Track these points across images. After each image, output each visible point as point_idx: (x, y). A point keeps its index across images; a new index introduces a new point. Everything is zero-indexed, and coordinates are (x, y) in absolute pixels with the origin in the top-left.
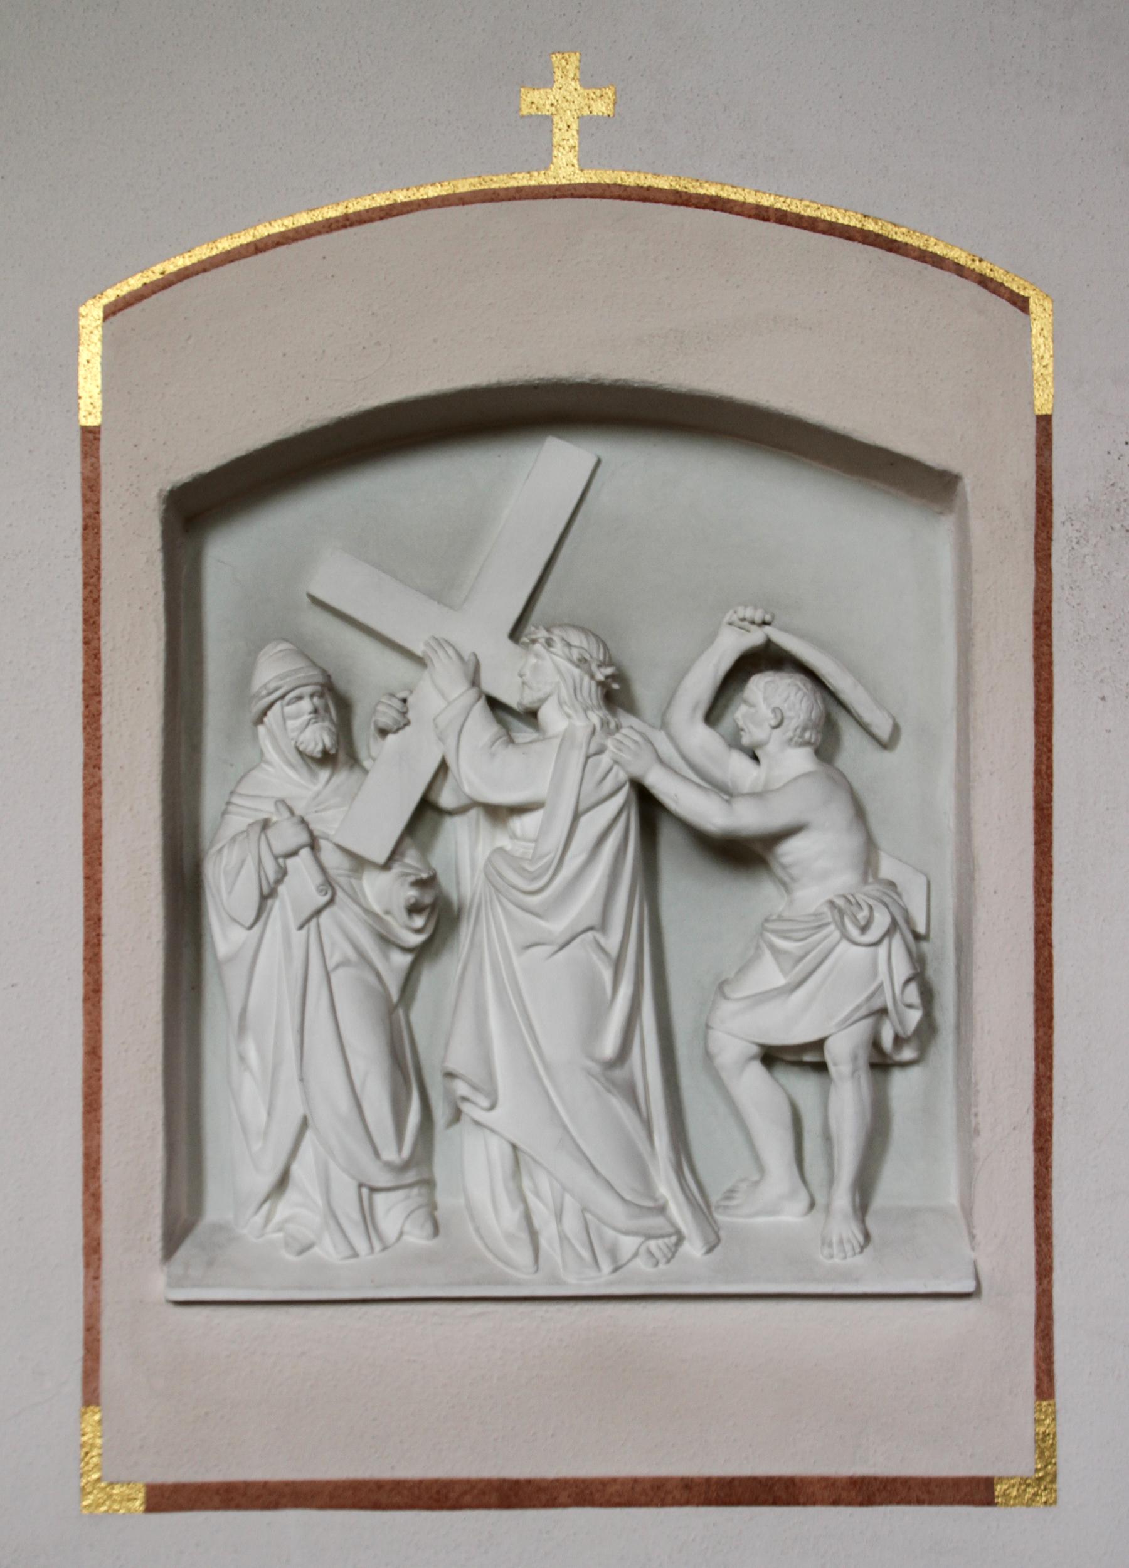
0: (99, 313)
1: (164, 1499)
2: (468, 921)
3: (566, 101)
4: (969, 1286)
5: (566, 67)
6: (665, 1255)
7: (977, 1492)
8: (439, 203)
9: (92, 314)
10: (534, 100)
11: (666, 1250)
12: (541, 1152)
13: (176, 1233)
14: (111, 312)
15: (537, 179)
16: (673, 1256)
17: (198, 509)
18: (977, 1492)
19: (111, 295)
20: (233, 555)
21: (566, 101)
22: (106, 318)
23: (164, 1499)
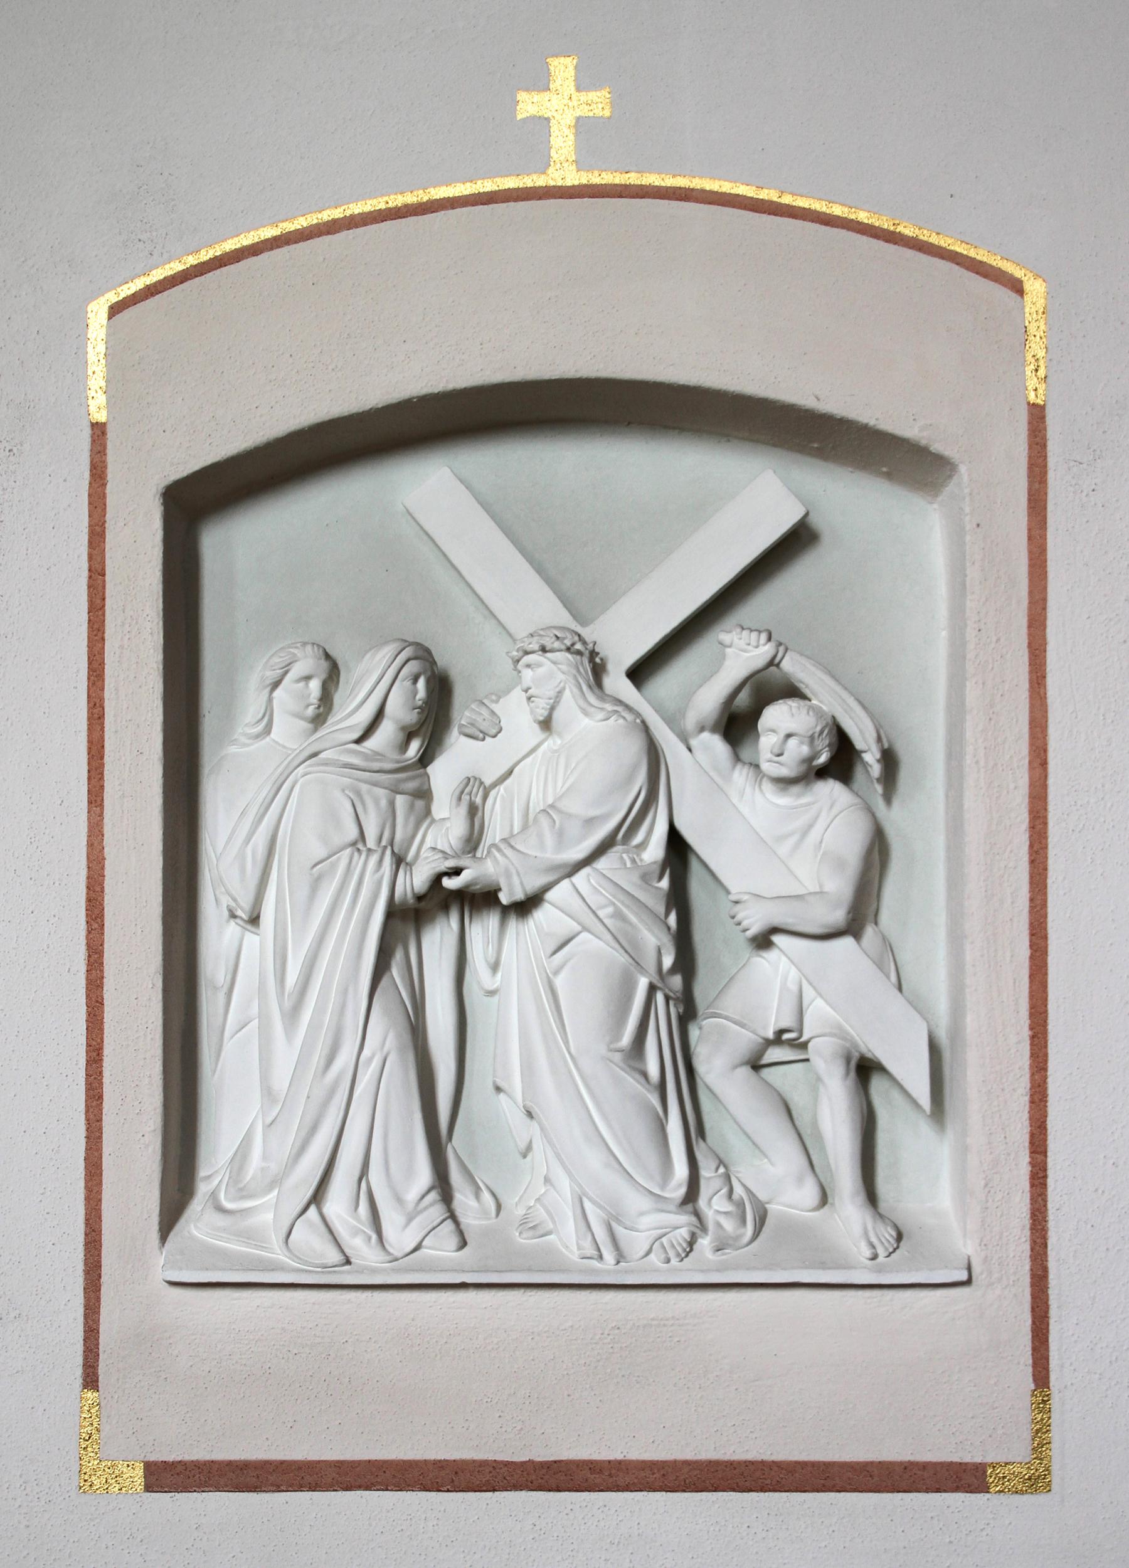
0: (104, 315)
1: (163, 1477)
2: (623, 903)
3: (562, 104)
4: (963, 1276)
5: (563, 69)
6: (685, 1250)
7: (966, 1478)
8: (95, 665)
9: (98, 312)
10: (528, 104)
11: (685, 1245)
12: (565, 1142)
13: (172, 1211)
14: (115, 310)
15: (540, 181)
16: (691, 1250)
17: (196, 503)
18: (966, 1478)
19: (112, 297)
20: (236, 545)
21: (562, 104)
22: (111, 315)
23: (163, 1477)
